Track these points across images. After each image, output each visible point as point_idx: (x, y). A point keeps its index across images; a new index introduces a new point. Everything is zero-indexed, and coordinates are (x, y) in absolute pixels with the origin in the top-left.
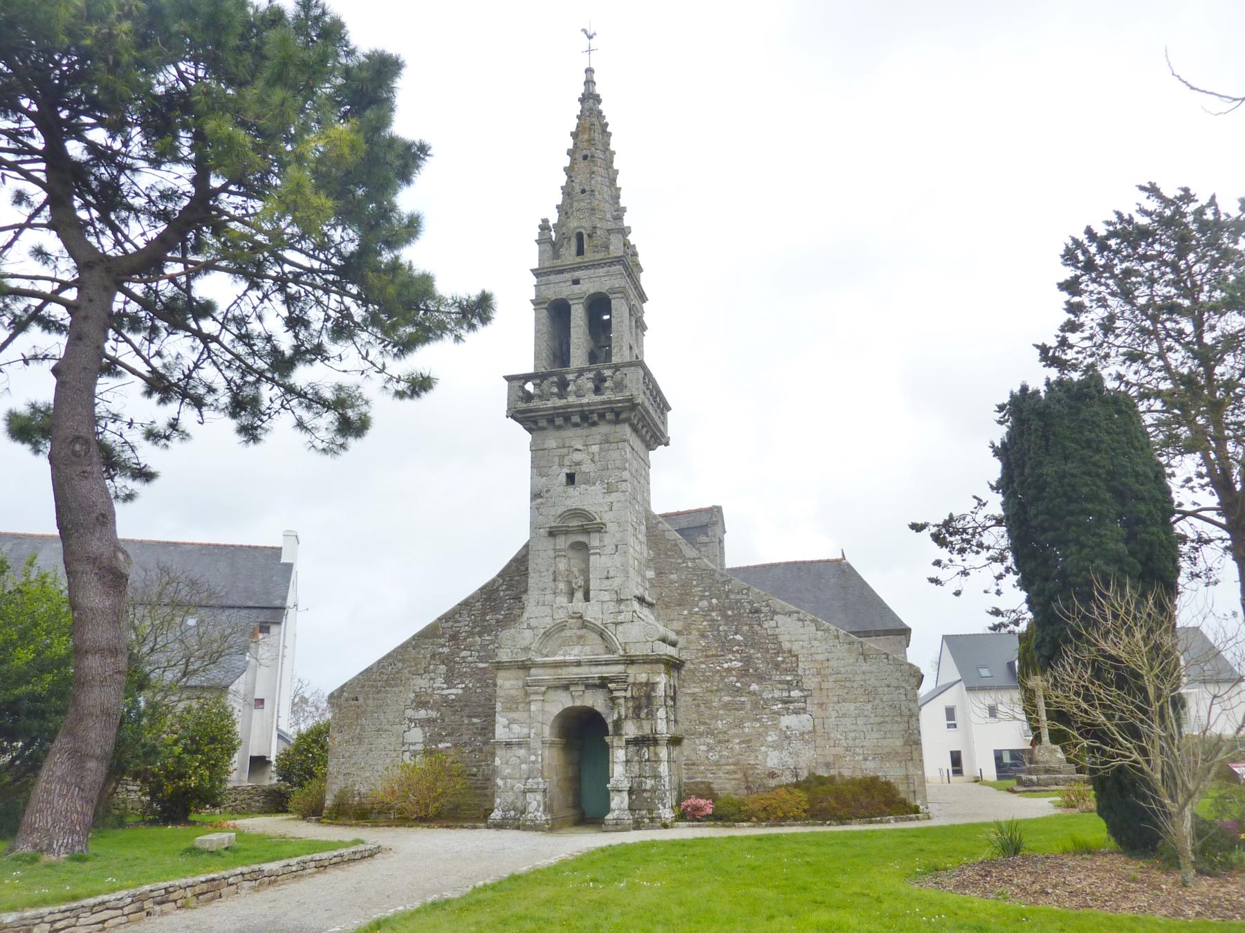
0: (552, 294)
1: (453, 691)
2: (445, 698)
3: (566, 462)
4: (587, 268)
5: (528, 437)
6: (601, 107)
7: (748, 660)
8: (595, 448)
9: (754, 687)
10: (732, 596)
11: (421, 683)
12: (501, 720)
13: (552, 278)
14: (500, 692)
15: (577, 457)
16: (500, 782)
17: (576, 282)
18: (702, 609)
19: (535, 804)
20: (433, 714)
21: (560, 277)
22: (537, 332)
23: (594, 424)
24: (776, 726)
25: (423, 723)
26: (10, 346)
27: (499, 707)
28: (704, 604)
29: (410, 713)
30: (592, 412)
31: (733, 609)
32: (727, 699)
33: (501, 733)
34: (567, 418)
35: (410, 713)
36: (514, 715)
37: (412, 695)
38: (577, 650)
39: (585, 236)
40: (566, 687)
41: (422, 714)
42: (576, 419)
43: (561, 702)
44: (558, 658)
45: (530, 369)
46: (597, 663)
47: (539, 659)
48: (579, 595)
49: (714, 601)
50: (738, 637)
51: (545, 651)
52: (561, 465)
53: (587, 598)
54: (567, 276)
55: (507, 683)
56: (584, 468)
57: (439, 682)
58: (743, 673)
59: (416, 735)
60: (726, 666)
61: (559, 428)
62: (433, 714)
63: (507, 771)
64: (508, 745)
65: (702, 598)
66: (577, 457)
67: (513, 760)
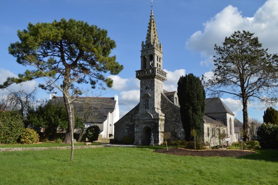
0: (143, 55)
1: (131, 124)
2: (130, 125)
3: (146, 85)
4: (149, 50)
5: (140, 81)
6: (111, 50)
7: (176, 119)
8: (150, 83)
9: (177, 124)
10: (174, 108)
11: (127, 122)
12: (136, 128)
13: (144, 52)
14: (135, 124)
15: (147, 84)
16: (135, 138)
17: (147, 53)
18: (169, 110)
19: (140, 141)
20: (129, 127)
21: (145, 52)
22: (141, 62)
23: (150, 79)
24: (180, 130)
25: (127, 129)
26: (58, 76)
27: (135, 126)
28: (170, 109)
29: (125, 127)
30: (149, 76)
31: (174, 110)
32: (173, 126)
33: (135, 130)
34: (145, 78)
35: (125, 127)
36: (137, 128)
37: (126, 124)
38: (146, 117)
39: (149, 44)
40: (145, 123)
41: (127, 127)
42: (147, 78)
43: (144, 126)
44: (144, 119)
45: (140, 69)
46: (149, 120)
47: (141, 119)
48: (147, 108)
49: (171, 109)
50: (175, 115)
51: (142, 117)
52: (145, 86)
53: (148, 109)
54: (146, 52)
55: (136, 122)
56: (148, 86)
57: (130, 122)
58: (176, 121)
59: (126, 131)
60: (173, 120)
61: (144, 79)
62: (129, 127)
63: (136, 136)
64: (136, 132)
65: (169, 108)
66: (147, 84)
67: (137, 135)
